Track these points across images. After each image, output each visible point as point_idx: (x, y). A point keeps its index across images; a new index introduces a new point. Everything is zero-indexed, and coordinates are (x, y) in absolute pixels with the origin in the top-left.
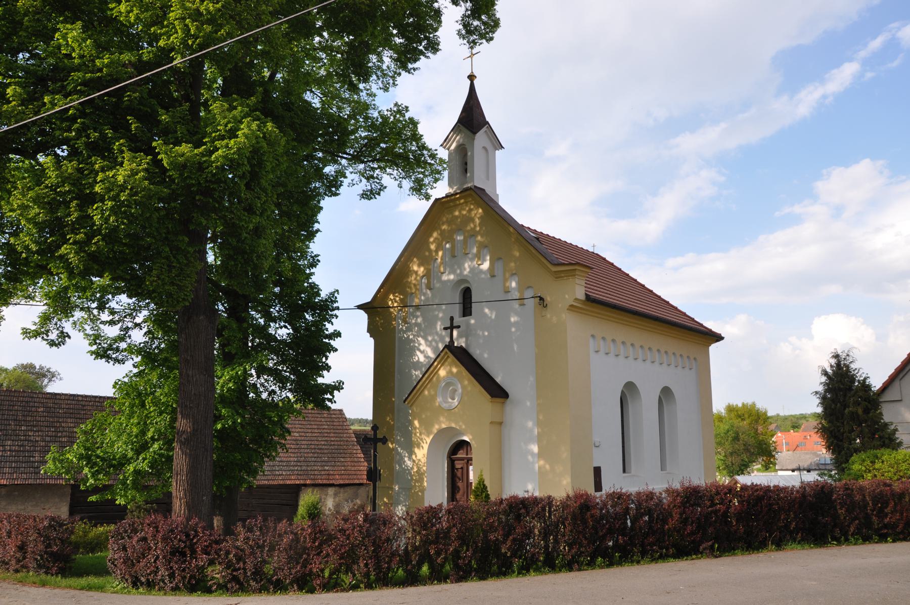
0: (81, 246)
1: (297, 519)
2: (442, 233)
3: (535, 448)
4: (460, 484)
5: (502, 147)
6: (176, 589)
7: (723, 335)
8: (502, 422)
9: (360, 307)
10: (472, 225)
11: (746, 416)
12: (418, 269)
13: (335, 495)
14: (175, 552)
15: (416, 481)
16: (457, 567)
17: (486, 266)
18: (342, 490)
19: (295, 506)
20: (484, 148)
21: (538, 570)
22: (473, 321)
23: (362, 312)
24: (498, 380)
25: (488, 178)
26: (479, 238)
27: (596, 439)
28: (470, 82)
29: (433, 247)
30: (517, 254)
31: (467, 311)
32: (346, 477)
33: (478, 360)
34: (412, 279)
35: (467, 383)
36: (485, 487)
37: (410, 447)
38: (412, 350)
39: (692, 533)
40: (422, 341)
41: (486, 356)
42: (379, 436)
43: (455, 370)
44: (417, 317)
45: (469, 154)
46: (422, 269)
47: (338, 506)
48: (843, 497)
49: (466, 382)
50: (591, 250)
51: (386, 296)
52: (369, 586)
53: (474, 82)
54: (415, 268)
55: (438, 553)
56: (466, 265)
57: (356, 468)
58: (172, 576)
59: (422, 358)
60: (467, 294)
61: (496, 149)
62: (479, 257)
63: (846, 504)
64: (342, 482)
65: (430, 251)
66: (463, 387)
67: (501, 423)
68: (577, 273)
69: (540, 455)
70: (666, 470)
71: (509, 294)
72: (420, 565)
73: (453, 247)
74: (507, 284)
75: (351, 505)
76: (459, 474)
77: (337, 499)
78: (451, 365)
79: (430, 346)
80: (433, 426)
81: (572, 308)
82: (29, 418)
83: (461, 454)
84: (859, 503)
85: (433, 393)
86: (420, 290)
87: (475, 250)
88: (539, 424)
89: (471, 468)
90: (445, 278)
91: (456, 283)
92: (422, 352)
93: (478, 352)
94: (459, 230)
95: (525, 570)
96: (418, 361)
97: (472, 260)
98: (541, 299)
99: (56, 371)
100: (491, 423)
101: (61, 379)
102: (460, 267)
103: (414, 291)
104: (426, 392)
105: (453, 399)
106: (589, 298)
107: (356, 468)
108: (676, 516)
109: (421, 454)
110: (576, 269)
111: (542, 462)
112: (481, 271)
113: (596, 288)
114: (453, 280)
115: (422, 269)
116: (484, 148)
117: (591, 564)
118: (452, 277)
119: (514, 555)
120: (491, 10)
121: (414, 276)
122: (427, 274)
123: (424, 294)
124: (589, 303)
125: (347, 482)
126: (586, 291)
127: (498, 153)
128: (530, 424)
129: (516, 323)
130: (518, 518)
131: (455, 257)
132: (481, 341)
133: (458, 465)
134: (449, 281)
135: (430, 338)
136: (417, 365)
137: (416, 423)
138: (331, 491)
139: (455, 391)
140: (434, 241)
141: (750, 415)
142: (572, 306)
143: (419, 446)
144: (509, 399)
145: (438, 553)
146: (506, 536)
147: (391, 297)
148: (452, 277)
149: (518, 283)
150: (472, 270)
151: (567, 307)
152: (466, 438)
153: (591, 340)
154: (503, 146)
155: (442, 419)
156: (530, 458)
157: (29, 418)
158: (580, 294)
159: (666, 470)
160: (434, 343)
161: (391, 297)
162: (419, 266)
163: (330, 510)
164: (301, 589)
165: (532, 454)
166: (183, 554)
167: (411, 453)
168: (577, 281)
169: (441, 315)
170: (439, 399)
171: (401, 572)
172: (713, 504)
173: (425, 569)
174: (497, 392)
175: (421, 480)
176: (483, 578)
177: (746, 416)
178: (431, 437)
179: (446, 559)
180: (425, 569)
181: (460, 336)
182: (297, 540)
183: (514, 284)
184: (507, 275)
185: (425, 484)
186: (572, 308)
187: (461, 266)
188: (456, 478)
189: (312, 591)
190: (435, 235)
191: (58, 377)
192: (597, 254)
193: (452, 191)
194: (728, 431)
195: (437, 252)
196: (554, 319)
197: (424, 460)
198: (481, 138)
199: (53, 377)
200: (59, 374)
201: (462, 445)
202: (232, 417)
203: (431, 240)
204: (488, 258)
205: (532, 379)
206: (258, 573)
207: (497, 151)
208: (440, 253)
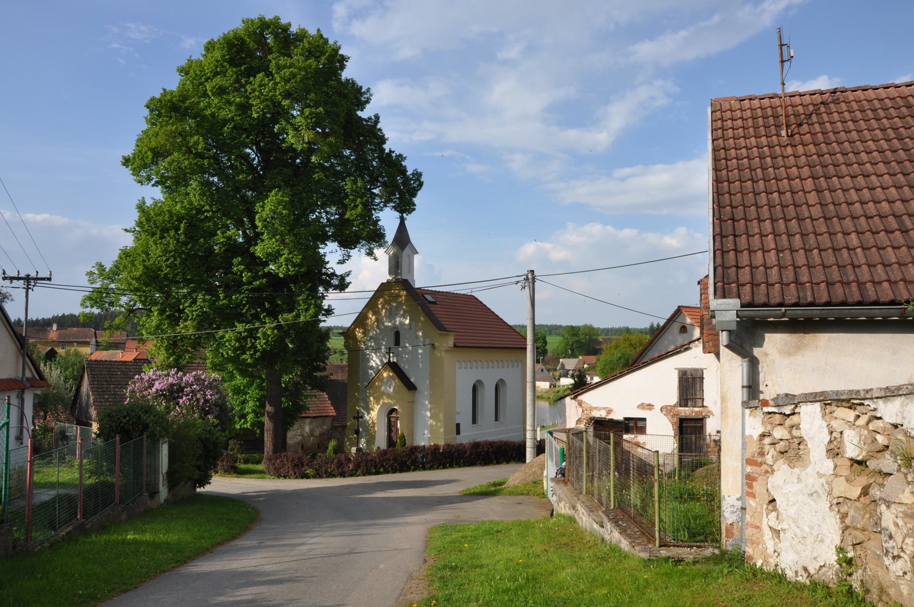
0: (252, 356)
1: (329, 451)
2: (385, 300)
3: (429, 414)
4: (393, 429)
6: (297, 478)
10: (400, 299)
11: (638, 345)
12: (372, 317)
13: (310, 423)
14: (296, 465)
15: (372, 427)
16: (392, 469)
17: (407, 322)
18: (315, 420)
19: (327, 448)
21: (419, 470)
22: (400, 349)
24: (412, 380)
25: (409, 272)
26: (404, 307)
27: (458, 410)
29: (380, 306)
30: (422, 319)
31: (397, 343)
32: (318, 411)
34: (369, 322)
35: (396, 382)
36: (404, 436)
37: (368, 410)
38: (368, 360)
39: (474, 458)
40: (374, 355)
41: (406, 367)
42: (360, 416)
43: (391, 374)
44: (371, 342)
46: (374, 317)
47: (312, 431)
49: (397, 381)
51: (354, 329)
52: (364, 475)
54: (371, 316)
55: (386, 465)
56: (397, 319)
57: (323, 405)
58: (295, 474)
59: (374, 365)
60: (397, 335)
62: (404, 316)
64: (315, 415)
65: (378, 307)
66: (396, 383)
67: (413, 402)
69: (431, 418)
72: (380, 468)
73: (390, 308)
74: (418, 333)
75: (320, 429)
76: (393, 424)
77: (311, 426)
78: (389, 371)
79: (378, 358)
80: (380, 400)
81: (447, 351)
82: (113, 380)
83: (394, 415)
85: (380, 384)
86: (373, 329)
87: (402, 312)
88: (430, 403)
89: (398, 421)
92: (374, 361)
93: (403, 365)
94: (395, 301)
95: (415, 470)
96: (372, 366)
97: (400, 317)
99: (8, 293)
101: (12, 300)
102: (394, 320)
103: (369, 328)
104: (377, 383)
105: (390, 388)
106: (455, 346)
107: (323, 405)
108: (468, 452)
109: (374, 414)
111: (431, 421)
112: (405, 324)
114: (390, 327)
115: (374, 317)
117: (438, 468)
118: (390, 324)
119: (411, 465)
121: (370, 320)
122: (377, 320)
123: (376, 331)
124: (456, 349)
125: (318, 415)
128: (427, 402)
129: (421, 354)
130: (413, 453)
131: (391, 315)
132: (404, 360)
133: (392, 420)
134: (388, 326)
135: (378, 354)
136: (372, 368)
137: (372, 398)
138: (308, 421)
139: (391, 384)
141: (641, 345)
143: (373, 410)
144: (417, 391)
145: (386, 465)
146: (408, 459)
147: (357, 329)
148: (390, 324)
149: (422, 333)
150: (400, 322)
152: (396, 407)
153: (457, 363)
155: (384, 397)
156: (426, 418)
157: (113, 380)
158: (451, 343)
160: (380, 358)
161: (357, 329)
162: (373, 315)
163: (307, 433)
164: (341, 477)
165: (428, 417)
166: (298, 466)
167: (369, 413)
169: (384, 343)
170: (383, 388)
171: (374, 470)
172: (483, 448)
173: (382, 470)
174: (411, 387)
175: (374, 427)
176: (401, 472)
177: (638, 345)
178: (379, 406)
179: (389, 467)
180: (382, 470)
181: (393, 356)
182: (339, 461)
183: (420, 334)
184: (418, 328)
185: (376, 429)
186: (447, 351)
187: (394, 319)
188: (391, 427)
189: (345, 477)
190: (381, 300)
191: (10, 298)
193: (391, 278)
194: (620, 358)
195: (382, 310)
196: (439, 354)
197: (375, 417)
198: (407, 250)
199: (4, 298)
200: (10, 296)
201: (393, 410)
202: (287, 402)
203: (379, 302)
204: (408, 318)
205: (428, 382)
206: (326, 472)
208: (384, 311)
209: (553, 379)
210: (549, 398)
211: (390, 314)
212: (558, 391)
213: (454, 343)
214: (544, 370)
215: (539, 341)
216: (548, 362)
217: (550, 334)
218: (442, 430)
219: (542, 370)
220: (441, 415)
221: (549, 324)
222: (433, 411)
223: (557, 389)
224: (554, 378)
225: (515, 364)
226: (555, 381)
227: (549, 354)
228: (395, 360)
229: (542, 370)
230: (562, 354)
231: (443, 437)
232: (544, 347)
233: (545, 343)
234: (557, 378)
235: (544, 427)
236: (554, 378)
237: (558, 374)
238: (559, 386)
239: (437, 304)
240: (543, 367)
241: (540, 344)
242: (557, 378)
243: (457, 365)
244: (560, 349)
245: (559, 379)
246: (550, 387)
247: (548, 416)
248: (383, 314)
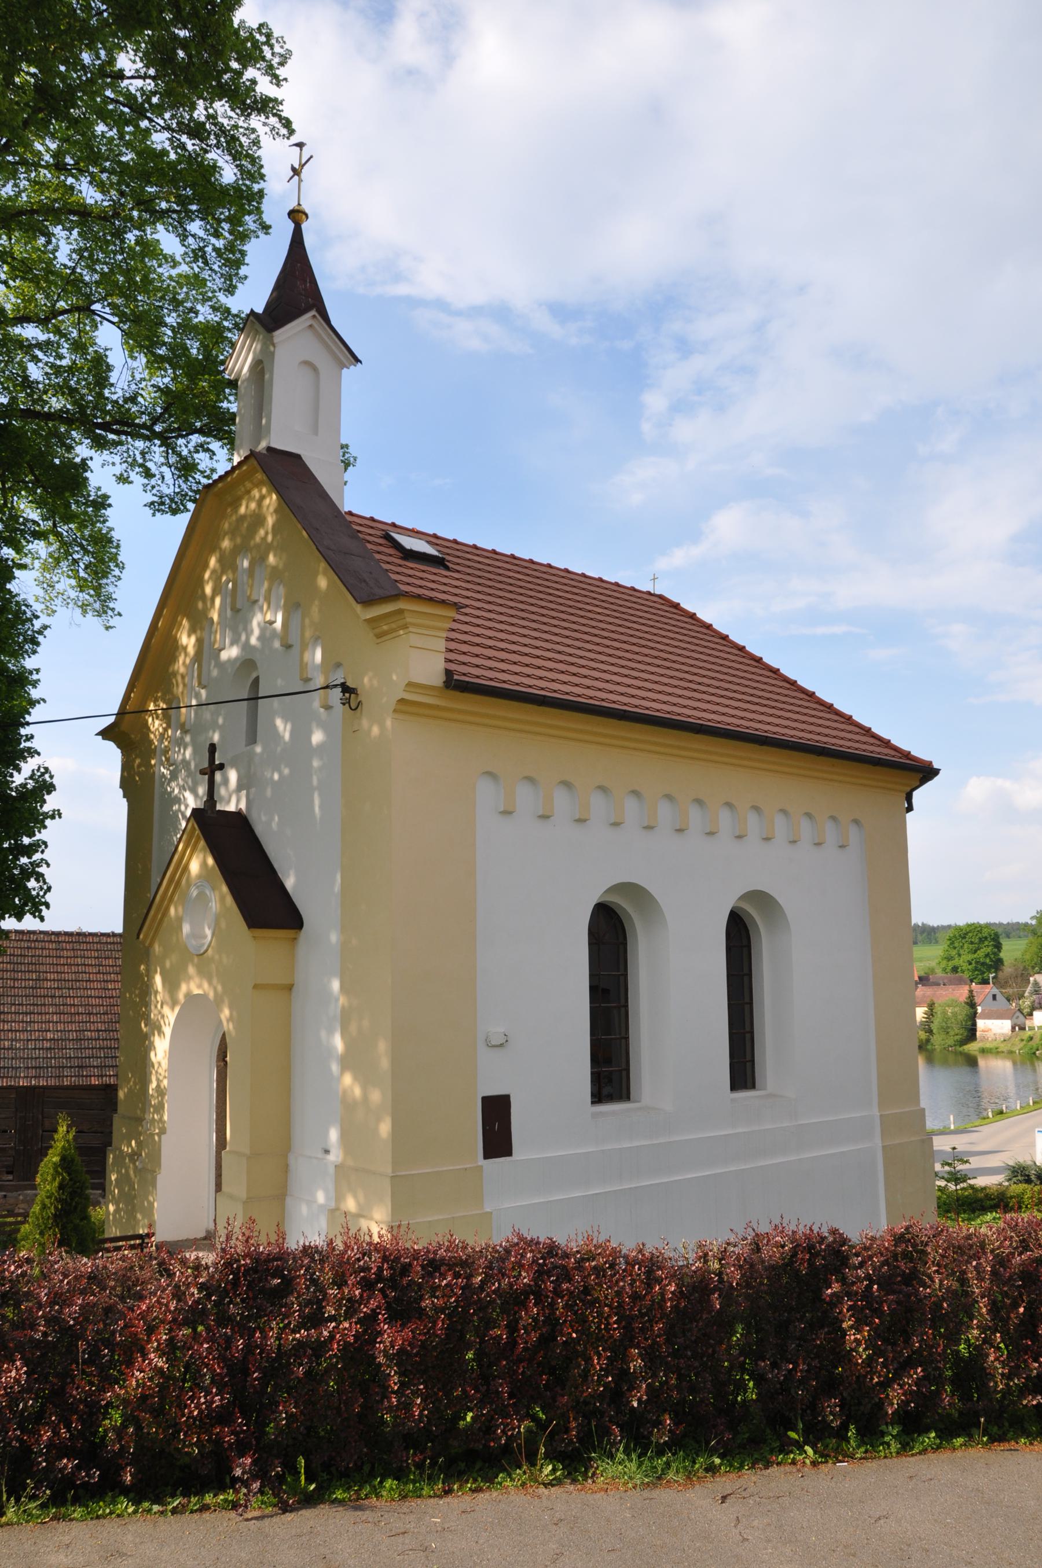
5: (357, 360)
7: (936, 766)
8: (293, 985)
9: (97, 735)
20: (307, 363)
23: (111, 746)
24: (290, 883)
28: (292, 226)
33: (260, 840)
45: (267, 376)
48: (869, 1287)
50: (644, 586)
53: (304, 226)
61: (343, 366)
63: (878, 1312)
67: (290, 988)
68: (409, 620)
70: (765, 1089)
71: (312, 683)
84: (938, 1306)
90: (224, 655)
91: (241, 665)
98: (345, 688)
100: (256, 987)
104: (172, 911)
106: (453, 683)
110: (400, 612)
113: (465, 648)
116: (307, 363)
120: (236, 32)
126: (448, 660)
127: (350, 375)
128: (336, 985)
132: (269, 792)
140: (210, 578)
142: (402, 701)
151: (392, 705)
154: (360, 358)
159: (765, 1089)
168: (415, 640)
178: (177, 1009)
192: (661, 597)
207: (345, 370)
209: (1018, 1014)
210: (1011, 1052)
211: (236, 610)
212: (1031, 1038)
213: (449, 673)
214: (999, 997)
215: (986, 943)
216: (1006, 982)
217: (1008, 936)
218: (385, 1128)
219: (994, 997)
220: (382, 1046)
221: (1005, 922)
222: (353, 1028)
223: (1028, 1033)
224: (1020, 1011)
225: (830, 832)
226: (1021, 1017)
227: (1008, 969)
228: (243, 806)
229: (994, 997)
230: (1033, 968)
231: (389, 1171)
232: (995, 954)
233: (998, 946)
234: (1026, 1011)
235: (1001, 1112)
236: (1020, 1011)
237: (1028, 1003)
238: (1032, 1029)
239: (447, 568)
240: (995, 991)
241: (989, 950)
242: (1026, 1011)
243: (486, 793)
244: (1028, 957)
245: (1031, 1014)
246: (1013, 1029)
247: (1012, 1090)
248: (215, 617)
